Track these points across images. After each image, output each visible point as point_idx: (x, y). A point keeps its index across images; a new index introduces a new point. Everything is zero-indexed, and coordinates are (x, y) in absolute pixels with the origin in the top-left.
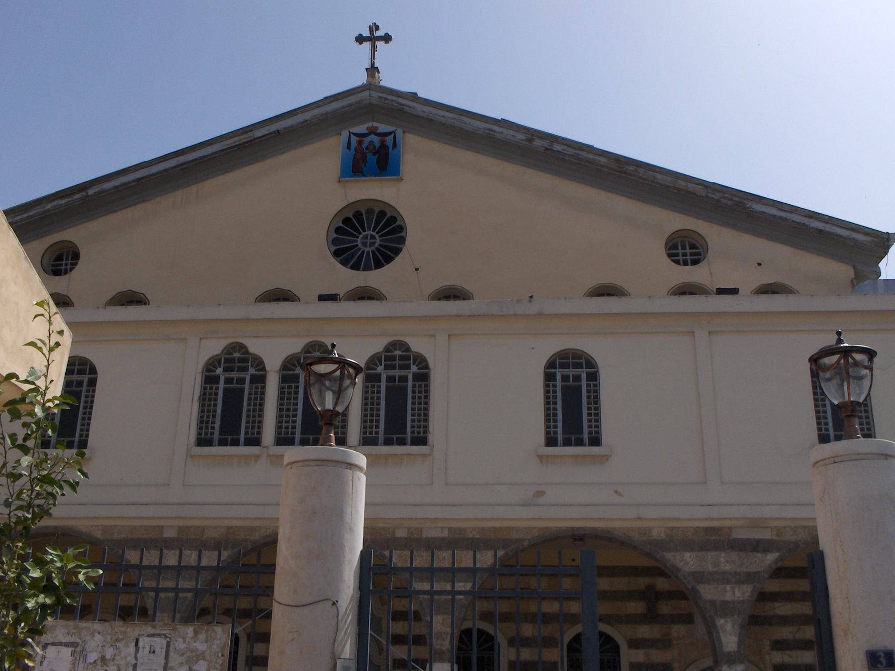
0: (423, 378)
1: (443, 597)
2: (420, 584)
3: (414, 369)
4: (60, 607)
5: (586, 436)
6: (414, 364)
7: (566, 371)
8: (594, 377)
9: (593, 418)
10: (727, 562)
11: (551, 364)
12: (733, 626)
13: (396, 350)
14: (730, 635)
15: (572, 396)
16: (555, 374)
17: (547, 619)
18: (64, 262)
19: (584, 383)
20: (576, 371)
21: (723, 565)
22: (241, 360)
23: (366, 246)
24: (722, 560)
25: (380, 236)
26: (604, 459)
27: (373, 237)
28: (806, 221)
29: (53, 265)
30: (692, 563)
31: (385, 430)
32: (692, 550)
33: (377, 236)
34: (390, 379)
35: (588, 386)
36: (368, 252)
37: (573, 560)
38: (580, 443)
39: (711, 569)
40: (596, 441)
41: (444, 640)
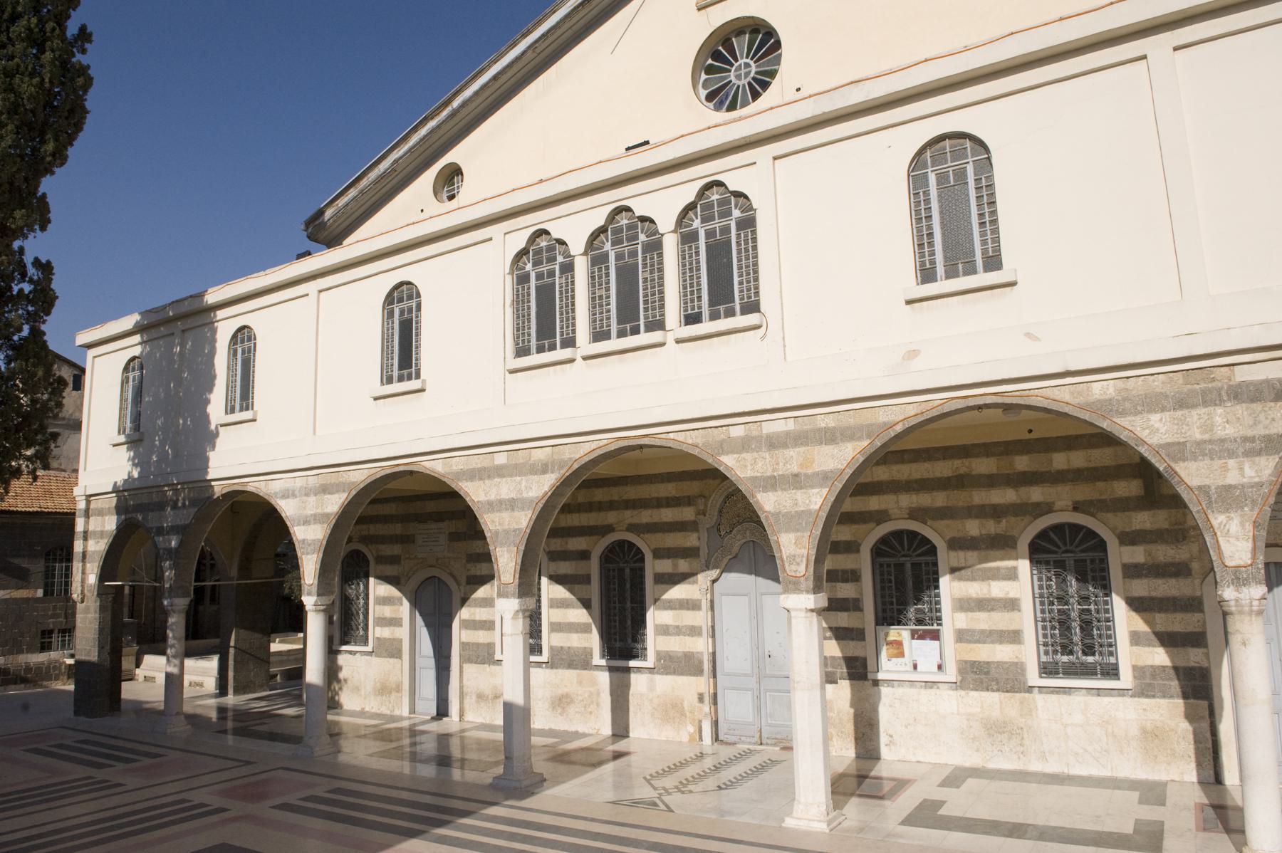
0: (748, 223)
2: (765, 494)
6: (736, 208)
8: (986, 165)
10: (1228, 422)
12: (1242, 524)
13: (713, 195)
14: (1238, 539)
17: (996, 512)
21: (1220, 428)
23: (740, 79)
24: (1218, 420)
25: (755, 62)
27: (747, 65)
30: (1163, 430)
31: (710, 300)
32: (1163, 409)
33: (752, 63)
34: (710, 234)
36: (744, 86)
37: (1030, 431)
39: (1198, 436)
41: (798, 564)
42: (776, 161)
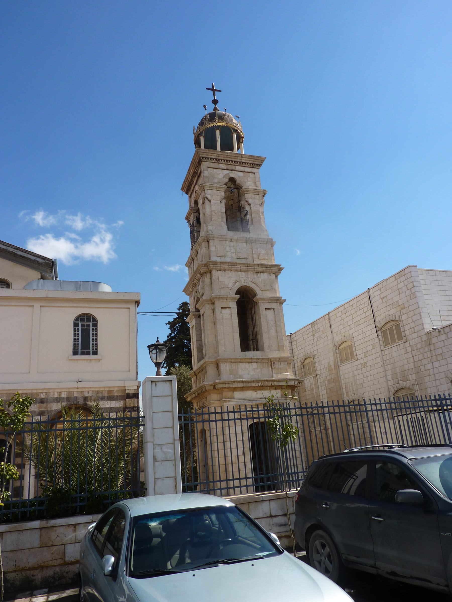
1: (252, 416)
5: (91, 351)
8: (95, 325)
11: (77, 319)
15: (86, 334)
16: (78, 323)
19: (91, 328)
20: (88, 323)
26: (99, 360)
28: (15, 251)
35: (93, 329)
38: (88, 354)
40: (95, 353)
42: (43, 308)
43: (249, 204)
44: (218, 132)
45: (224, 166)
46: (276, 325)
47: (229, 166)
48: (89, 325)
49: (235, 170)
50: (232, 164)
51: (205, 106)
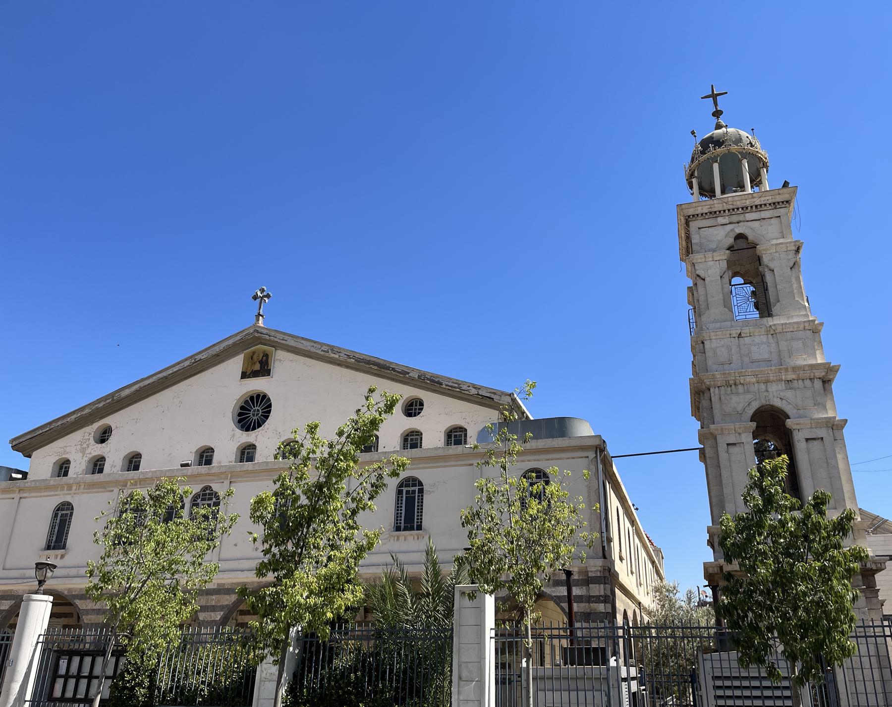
3: (214, 500)
4: (490, 602)
7: (409, 489)
8: (421, 491)
9: (420, 514)
18: (107, 435)
22: (210, 494)
29: (102, 437)
38: (412, 529)
40: (419, 528)
43: (770, 270)
44: (716, 166)
45: (726, 220)
46: (828, 464)
47: (766, 212)
48: (414, 492)
49: (744, 221)
50: (738, 212)
51: (693, 133)
